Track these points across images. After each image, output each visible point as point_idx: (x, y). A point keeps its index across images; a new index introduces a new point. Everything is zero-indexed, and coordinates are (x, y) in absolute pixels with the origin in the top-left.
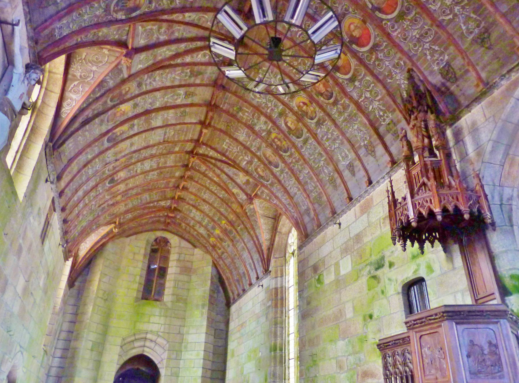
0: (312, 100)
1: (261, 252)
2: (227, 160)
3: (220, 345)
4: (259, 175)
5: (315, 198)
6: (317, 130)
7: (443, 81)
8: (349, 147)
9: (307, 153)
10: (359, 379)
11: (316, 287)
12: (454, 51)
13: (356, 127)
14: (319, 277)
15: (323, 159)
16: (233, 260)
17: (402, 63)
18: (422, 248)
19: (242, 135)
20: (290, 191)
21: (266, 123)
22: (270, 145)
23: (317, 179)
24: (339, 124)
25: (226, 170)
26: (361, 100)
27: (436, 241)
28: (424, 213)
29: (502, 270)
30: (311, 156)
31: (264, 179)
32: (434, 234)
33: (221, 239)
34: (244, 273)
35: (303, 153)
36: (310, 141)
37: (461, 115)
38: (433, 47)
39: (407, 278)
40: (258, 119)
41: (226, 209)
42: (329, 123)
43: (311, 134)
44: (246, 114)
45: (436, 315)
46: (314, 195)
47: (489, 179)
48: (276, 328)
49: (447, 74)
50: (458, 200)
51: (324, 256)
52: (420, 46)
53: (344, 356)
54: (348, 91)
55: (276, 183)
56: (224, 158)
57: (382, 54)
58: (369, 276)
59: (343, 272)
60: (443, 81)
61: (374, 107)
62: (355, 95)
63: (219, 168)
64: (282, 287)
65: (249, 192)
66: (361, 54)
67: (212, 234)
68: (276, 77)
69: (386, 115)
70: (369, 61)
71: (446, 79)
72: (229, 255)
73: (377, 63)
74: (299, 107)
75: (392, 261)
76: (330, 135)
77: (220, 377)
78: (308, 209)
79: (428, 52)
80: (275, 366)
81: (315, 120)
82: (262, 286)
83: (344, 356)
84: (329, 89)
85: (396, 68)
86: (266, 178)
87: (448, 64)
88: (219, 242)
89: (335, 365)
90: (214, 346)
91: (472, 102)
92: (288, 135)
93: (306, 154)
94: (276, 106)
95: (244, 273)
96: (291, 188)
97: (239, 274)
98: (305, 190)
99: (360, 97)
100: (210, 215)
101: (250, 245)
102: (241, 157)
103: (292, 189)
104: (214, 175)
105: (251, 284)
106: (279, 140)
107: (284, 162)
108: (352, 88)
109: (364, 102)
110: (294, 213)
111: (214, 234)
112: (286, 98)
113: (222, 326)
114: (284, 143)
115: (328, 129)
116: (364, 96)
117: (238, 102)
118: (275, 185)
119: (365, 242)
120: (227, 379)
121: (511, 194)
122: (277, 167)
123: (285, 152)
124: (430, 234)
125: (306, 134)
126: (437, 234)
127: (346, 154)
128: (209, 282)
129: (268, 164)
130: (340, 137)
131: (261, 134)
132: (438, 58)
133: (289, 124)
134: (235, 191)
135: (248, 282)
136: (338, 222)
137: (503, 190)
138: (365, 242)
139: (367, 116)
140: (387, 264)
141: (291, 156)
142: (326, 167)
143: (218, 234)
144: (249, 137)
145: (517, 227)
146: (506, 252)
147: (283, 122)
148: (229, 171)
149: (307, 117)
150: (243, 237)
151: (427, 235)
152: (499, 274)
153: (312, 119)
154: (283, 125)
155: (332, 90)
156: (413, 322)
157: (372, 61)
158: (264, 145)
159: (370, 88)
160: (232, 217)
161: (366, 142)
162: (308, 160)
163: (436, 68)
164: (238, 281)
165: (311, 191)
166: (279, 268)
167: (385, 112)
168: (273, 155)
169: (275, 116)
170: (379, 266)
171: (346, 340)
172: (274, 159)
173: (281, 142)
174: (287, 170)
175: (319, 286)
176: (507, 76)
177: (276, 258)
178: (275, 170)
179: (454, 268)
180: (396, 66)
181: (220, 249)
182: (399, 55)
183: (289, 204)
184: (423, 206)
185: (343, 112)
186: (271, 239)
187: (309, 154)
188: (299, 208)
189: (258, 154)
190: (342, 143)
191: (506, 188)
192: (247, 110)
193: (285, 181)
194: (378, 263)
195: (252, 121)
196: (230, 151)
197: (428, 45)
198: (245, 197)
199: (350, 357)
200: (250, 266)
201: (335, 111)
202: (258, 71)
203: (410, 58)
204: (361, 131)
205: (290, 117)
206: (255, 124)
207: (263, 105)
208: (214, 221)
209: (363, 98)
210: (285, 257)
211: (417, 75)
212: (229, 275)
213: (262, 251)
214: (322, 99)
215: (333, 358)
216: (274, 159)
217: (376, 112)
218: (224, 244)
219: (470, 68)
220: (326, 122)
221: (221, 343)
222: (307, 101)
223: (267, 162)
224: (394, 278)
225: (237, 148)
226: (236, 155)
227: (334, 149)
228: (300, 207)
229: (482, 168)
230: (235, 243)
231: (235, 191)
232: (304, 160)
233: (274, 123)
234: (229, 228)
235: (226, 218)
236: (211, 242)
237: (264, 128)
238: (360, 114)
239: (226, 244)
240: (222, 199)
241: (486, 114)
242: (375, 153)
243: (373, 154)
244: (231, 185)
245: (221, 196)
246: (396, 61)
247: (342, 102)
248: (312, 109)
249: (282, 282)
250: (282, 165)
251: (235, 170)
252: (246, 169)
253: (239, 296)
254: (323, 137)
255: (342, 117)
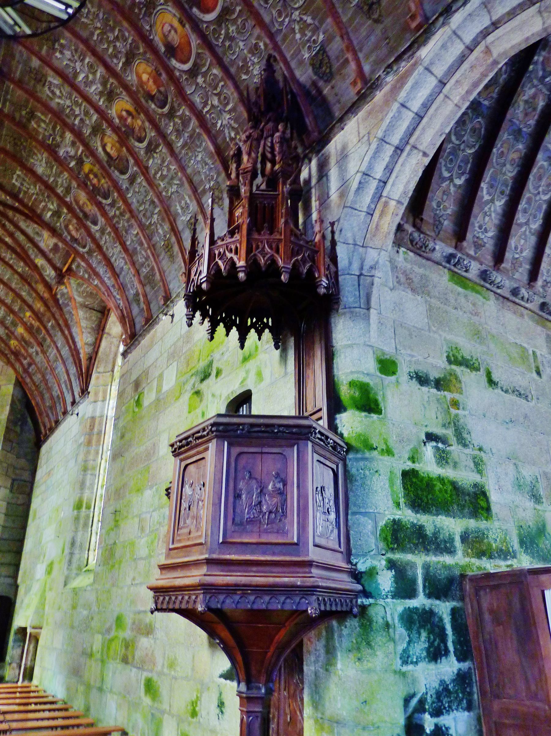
0: (140, 108)
1: (77, 362)
2: (21, 208)
3: (19, 502)
4: (72, 237)
5: (146, 277)
6: (148, 160)
7: (315, 78)
8: (190, 192)
9: (134, 200)
10: (160, 546)
11: (134, 412)
12: (332, 27)
13: (199, 158)
14: (139, 397)
15: (157, 210)
16: (43, 376)
17: (261, 44)
18: (242, 340)
19: (40, 164)
20: (115, 265)
21: (73, 144)
22: (83, 185)
23: (148, 244)
24: (177, 151)
25: (22, 225)
26: (206, 110)
27: (267, 331)
28: (223, 268)
29: (340, 373)
30: (140, 206)
31: (79, 244)
32: (265, 320)
33: (26, 342)
34: (58, 396)
35: (130, 201)
36: (139, 180)
37: (332, 135)
38: (305, 18)
39: (232, 393)
40: (62, 136)
41: (29, 294)
42: (163, 149)
43: (139, 167)
44: (43, 125)
45: (204, 430)
46: (144, 271)
47: (349, 235)
48: (85, 475)
49: (320, 67)
50: (277, 251)
51: (148, 365)
52: (286, 16)
53: (149, 512)
54: (188, 92)
55: (95, 252)
56: (17, 204)
57: (234, 28)
58: (193, 391)
59: (166, 387)
60: (315, 78)
61: (224, 123)
62: (197, 100)
63: (11, 221)
64: (101, 417)
65: (58, 265)
66: (205, 26)
67: (13, 333)
68: (82, 61)
69: (238, 137)
70: (217, 39)
71: (319, 76)
72: (38, 368)
73: (227, 44)
74: (120, 117)
75: (221, 367)
76: (166, 169)
77: (15, 549)
78: (137, 294)
79: (297, 27)
80: (76, 531)
81: (145, 143)
82: (77, 414)
83: (149, 512)
84: (162, 89)
85: (253, 55)
86: (81, 241)
87: (323, 50)
88: (24, 348)
89: (137, 526)
90: (8, 503)
91: (347, 113)
92: (107, 167)
93: (134, 201)
94: (86, 113)
95: (58, 396)
96: (116, 260)
97: (52, 398)
98: (133, 264)
99: (205, 104)
100: (6, 301)
101: (65, 351)
102: (43, 204)
103: (117, 261)
104: (5, 233)
105: (65, 413)
106: (96, 176)
107: (104, 214)
108: (194, 87)
109: (210, 115)
110: (119, 300)
111: (16, 334)
112: (102, 100)
113: (26, 476)
114: (103, 181)
115: (163, 161)
116: (209, 102)
117: (27, 101)
118: (95, 254)
119: (195, 341)
120: (24, 553)
121: (376, 259)
122: (95, 223)
123: (106, 198)
124: (260, 319)
125: (133, 168)
126: (270, 320)
127: (186, 203)
128: (8, 408)
129: (83, 220)
130: (179, 174)
131: (69, 163)
132: (311, 37)
133: (108, 149)
134: (40, 261)
135: (63, 410)
136: (171, 313)
137: (366, 253)
138: (195, 341)
139: (213, 139)
140: (214, 373)
141: (112, 205)
142: (161, 225)
143: (21, 334)
144: (52, 168)
145: (375, 311)
146: (351, 346)
147: (99, 144)
148: (28, 226)
149: (133, 138)
150: (55, 339)
151: (254, 320)
152: (336, 379)
153: (141, 140)
154: (100, 149)
155: (166, 91)
156: (178, 444)
157: (221, 40)
158: (74, 184)
159: (219, 90)
160: (39, 305)
161: (212, 183)
162: (136, 212)
163: (307, 56)
164: (51, 408)
165: (142, 265)
166: (101, 388)
167: (237, 133)
168: (88, 203)
169: (87, 131)
170: (205, 376)
171: (154, 489)
172: (91, 209)
173: (99, 181)
174: (109, 229)
175: (136, 410)
176: (395, 68)
177: (99, 373)
178: (94, 228)
179: (286, 374)
180: (254, 50)
181: (25, 359)
182: (257, 31)
183: (113, 286)
184: (222, 256)
185: (183, 130)
186: (95, 343)
187: (138, 202)
188: (127, 293)
189: (68, 199)
190: (181, 185)
191: (371, 250)
192: (43, 117)
193: (107, 249)
194: (205, 372)
195: (53, 139)
196: (26, 193)
197: (297, 13)
198: (53, 273)
199: (154, 513)
200: (66, 386)
201: (171, 128)
202: (54, 45)
203: (272, 36)
204: (206, 164)
205: (110, 137)
206: (58, 146)
207: (68, 111)
208: (12, 311)
209: (208, 108)
210: (113, 371)
211: (280, 67)
212: (38, 399)
213: (80, 361)
214: (153, 106)
215: (136, 516)
216: (91, 209)
217: (226, 131)
218: (30, 350)
219: (349, 56)
220: (160, 148)
221: (21, 499)
222: (131, 108)
223: (81, 215)
224: (218, 393)
225: (35, 186)
226: (35, 199)
227: (172, 193)
228: (128, 290)
229: (343, 216)
230: (45, 348)
231: (40, 261)
232: (131, 211)
233: (86, 145)
234: (36, 324)
235: (30, 308)
236: (12, 347)
237: (72, 153)
238: (205, 137)
239: (34, 350)
240: (21, 276)
241: (361, 131)
242: (223, 201)
243: (220, 203)
244: (32, 252)
245: (20, 270)
246: (254, 42)
247: (181, 112)
248: (139, 122)
249: (103, 408)
250: (101, 220)
251: (36, 226)
252: (52, 225)
253: (52, 430)
254: (156, 173)
255: (182, 140)
